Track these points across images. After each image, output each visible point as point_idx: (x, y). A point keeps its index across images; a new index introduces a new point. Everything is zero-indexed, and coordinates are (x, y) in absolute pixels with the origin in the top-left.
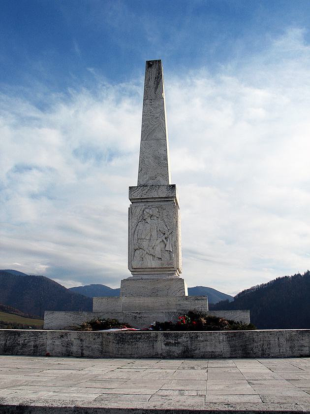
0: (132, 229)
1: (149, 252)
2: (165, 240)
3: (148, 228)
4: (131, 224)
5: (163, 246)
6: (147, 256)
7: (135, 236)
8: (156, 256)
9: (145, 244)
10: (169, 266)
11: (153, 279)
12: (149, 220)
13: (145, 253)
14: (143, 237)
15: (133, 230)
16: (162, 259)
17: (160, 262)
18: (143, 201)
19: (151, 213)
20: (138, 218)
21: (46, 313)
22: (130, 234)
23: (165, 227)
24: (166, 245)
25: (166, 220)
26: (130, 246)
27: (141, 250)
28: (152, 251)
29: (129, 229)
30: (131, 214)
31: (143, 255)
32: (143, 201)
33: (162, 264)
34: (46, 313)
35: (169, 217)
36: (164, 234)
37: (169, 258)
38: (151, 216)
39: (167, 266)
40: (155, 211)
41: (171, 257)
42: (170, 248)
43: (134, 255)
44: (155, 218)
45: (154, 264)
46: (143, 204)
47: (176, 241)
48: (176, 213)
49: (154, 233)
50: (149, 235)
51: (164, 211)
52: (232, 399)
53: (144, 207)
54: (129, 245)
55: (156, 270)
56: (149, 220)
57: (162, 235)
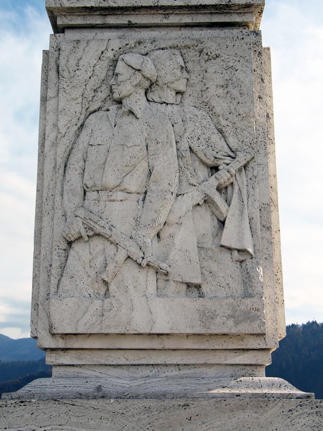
0: (54, 144)
1: (137, 254)
2: (218, 199)
3: (140, 140)
4: (51, 118)
5: (207, 223)
6: (130, 273)
7: (73, 175)
8: (174, 274)
9: (119, 214)
10: (245, 328)
11: (162, 396)
12: (137, 102)
13: (122, 255)
14: (111, 180)
15: (61, 149)
16: (205, 289)
17: (191, 304)
18: (111, 20)
19: (150, 69)
20: (89, 94)
21: (3, 394)
22: (48, 167)
23: (216, 138)
24: (222, 223)
25: (220, 106)
26: (46, 219)
27: (98, 244)
28: (153, 251)
29: (42, 145)
30: (52, 74)
31: (111, 267)
32: (111, 20)
33: (207, 316)
34: (3, 394)
35: (235, 92)
36: (215, 169)
37: (237, 287)
38: (151, 86)
39: (229, 327)
40: (167, 67)
41: (248, 280)
42: (240, 235)
43: (63, 267)
44: (170, 96)
45: (167, 313)
46: (108, 34)
47: (268, 208)
48: (263, 77)
49: (166, 162)
50: (143, 167)
51: (213, 66)
52: (101, 353)
53: (116, 44)
54: (39, 218)
55: (169, 344)
56: (137, 102)
57: (203, 172)
